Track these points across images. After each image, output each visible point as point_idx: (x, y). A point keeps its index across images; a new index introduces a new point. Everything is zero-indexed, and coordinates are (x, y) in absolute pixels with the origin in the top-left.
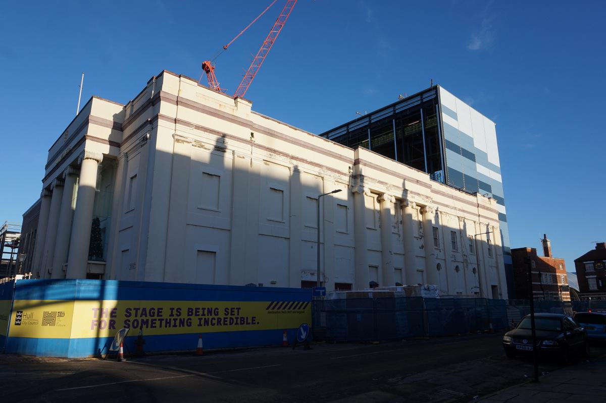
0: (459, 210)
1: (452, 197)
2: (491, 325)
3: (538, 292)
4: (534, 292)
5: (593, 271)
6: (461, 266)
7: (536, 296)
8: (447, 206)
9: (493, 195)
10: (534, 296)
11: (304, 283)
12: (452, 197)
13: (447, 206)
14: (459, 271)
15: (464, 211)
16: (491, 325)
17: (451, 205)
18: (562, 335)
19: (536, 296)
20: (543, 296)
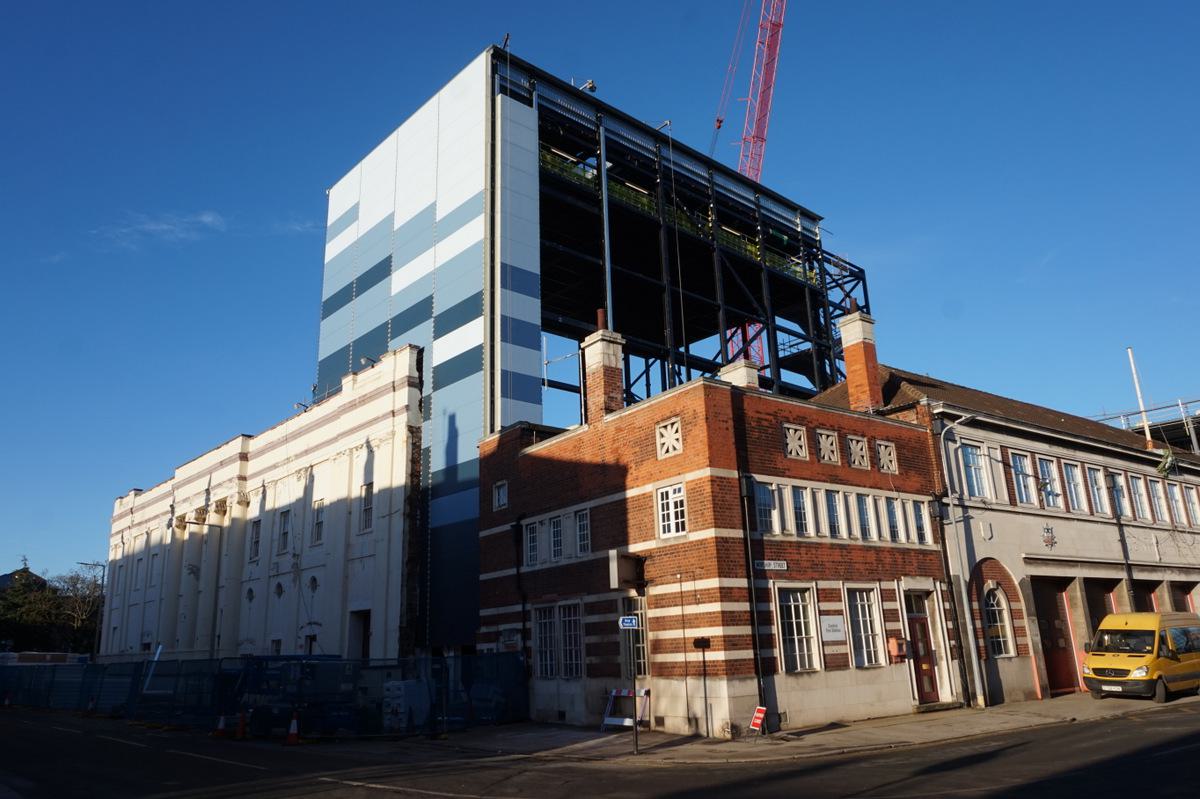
0: (297, 456)
1: (286, 440)
2: (294, 723)
3: (502, 610)
4: (483, 613)
5: (978, 559)
6: (286, 581)
7: (493, 629)
8: (275, 467)
9: (429, 397)
10: (484, 630)
11: (820, 449)
12: (286, 440)
13: (275, 467)
14: (254, 600)
15: (306, 452)
16: (294, 723)
17: (278, 460)
18: (418, 522)
19: (493, 629)
20: (519, 626)
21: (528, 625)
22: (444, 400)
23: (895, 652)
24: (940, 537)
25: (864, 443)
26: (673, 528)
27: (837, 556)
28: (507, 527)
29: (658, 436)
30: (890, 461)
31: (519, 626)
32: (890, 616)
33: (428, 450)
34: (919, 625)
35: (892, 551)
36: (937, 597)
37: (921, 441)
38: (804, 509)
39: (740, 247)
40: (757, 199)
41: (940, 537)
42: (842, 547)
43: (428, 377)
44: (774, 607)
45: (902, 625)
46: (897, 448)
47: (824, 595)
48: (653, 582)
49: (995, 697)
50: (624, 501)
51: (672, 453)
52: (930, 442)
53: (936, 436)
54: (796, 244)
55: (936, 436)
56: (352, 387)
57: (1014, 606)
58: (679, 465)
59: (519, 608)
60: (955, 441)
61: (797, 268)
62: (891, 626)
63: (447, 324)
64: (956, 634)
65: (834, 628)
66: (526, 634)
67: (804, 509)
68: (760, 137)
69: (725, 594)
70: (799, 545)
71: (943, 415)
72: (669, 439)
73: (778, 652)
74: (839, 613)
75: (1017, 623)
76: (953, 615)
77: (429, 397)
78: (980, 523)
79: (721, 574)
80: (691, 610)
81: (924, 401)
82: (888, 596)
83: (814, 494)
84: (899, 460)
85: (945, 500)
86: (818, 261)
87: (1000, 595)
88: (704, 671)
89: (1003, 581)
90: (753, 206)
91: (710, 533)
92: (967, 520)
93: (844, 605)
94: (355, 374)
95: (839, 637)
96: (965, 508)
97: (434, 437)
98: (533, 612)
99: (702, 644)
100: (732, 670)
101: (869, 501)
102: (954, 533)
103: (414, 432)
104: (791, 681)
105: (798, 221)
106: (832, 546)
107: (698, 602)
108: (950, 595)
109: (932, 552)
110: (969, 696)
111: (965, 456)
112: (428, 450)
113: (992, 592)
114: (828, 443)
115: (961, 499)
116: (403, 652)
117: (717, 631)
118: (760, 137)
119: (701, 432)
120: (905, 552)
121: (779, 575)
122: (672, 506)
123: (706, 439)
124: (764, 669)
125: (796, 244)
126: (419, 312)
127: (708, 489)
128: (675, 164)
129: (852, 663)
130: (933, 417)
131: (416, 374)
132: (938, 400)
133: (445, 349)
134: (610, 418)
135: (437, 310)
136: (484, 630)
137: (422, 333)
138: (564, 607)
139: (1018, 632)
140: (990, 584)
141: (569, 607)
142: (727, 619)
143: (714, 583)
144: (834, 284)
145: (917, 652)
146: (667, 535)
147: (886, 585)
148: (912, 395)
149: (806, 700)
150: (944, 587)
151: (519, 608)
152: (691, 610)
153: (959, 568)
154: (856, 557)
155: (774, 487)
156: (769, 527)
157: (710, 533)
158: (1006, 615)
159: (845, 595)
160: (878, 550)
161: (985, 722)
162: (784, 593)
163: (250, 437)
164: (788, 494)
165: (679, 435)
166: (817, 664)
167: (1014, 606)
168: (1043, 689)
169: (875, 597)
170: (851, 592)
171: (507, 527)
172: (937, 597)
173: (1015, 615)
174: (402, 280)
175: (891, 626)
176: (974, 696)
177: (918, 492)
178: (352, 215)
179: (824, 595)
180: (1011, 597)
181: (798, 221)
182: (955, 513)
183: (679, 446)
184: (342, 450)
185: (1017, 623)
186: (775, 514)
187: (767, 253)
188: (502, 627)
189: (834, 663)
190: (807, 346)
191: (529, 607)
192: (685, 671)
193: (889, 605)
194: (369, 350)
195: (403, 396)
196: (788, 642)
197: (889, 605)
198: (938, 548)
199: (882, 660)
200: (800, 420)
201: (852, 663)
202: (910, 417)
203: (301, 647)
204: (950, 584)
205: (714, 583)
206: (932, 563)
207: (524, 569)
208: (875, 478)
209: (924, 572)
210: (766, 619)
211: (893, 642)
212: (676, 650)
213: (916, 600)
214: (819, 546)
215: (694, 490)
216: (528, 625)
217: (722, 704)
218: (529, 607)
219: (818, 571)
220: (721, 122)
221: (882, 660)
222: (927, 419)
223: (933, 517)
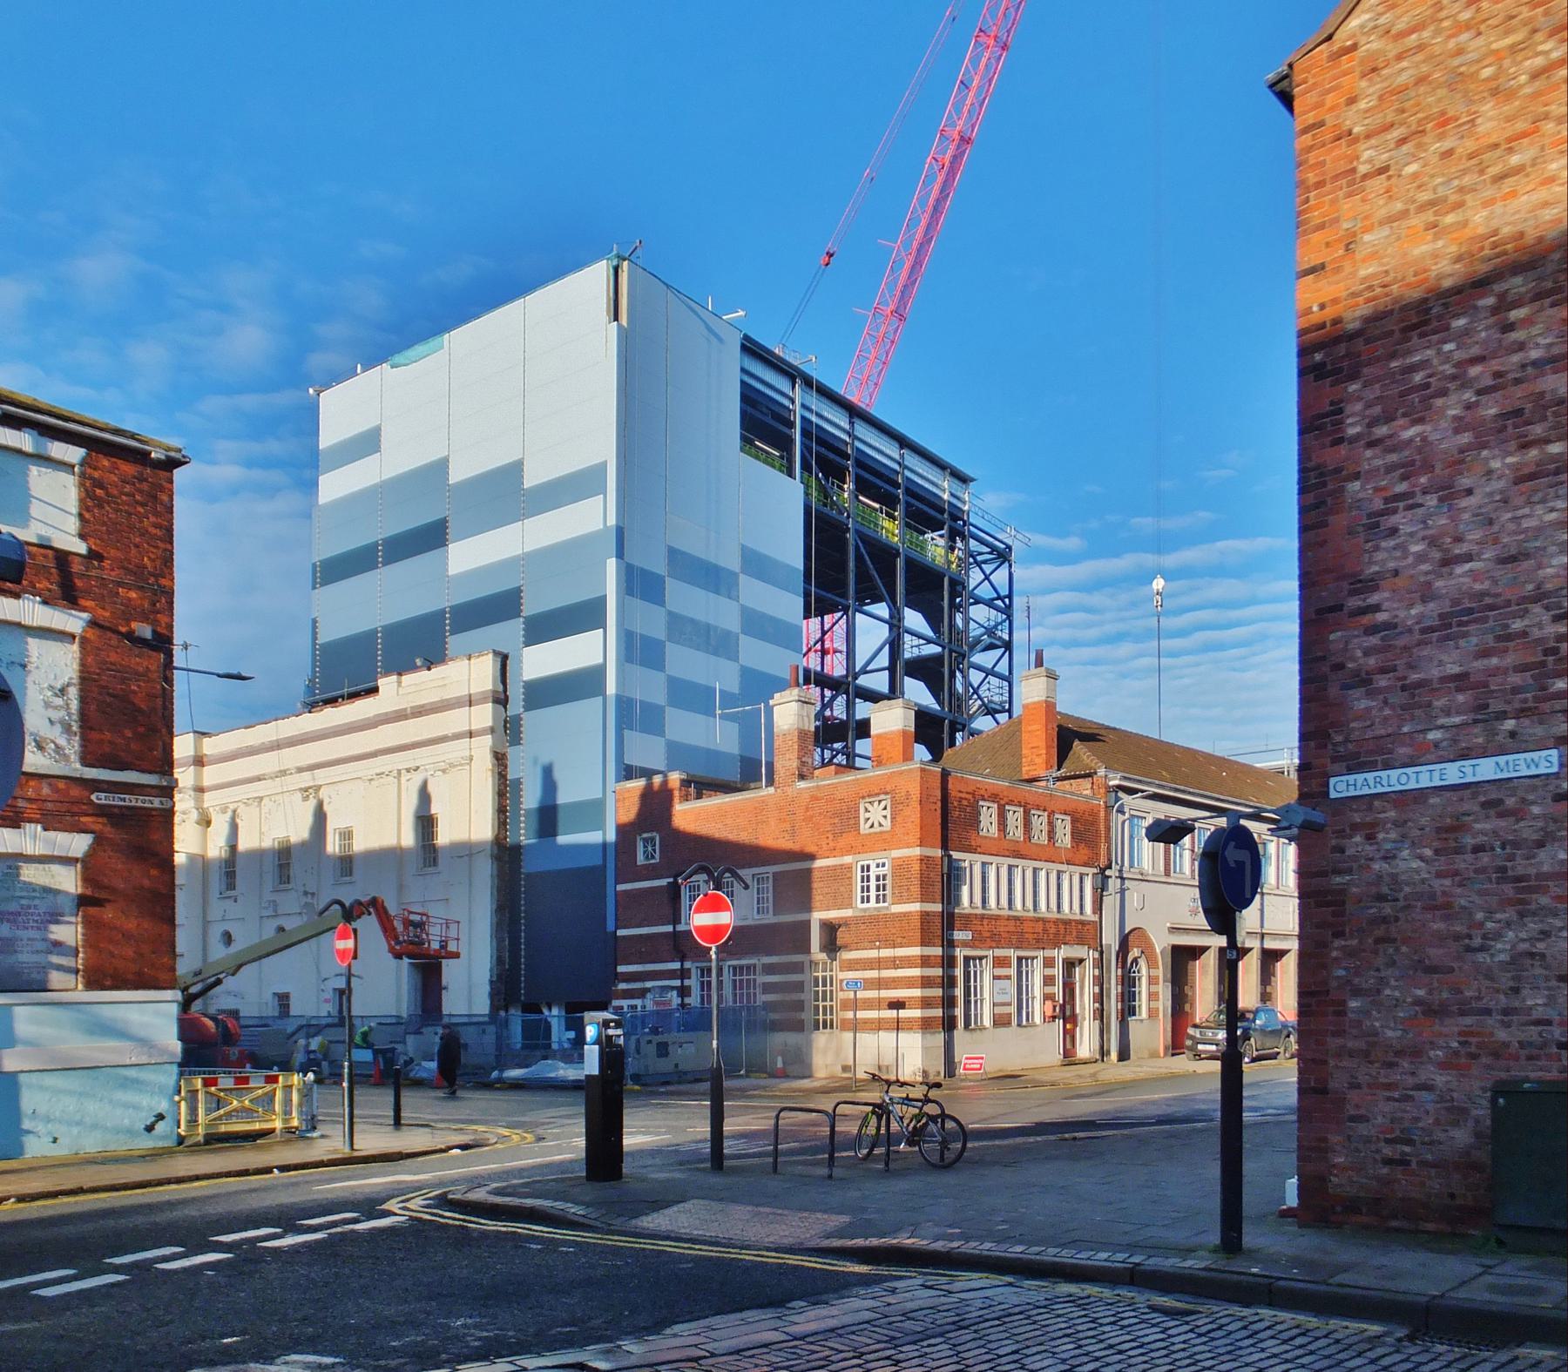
4: (620, 969)
10: (622, 986)
20: (677, 983)
21: (687, 982)
22: (534, 723)
23: (1049, 1013)
24: (1098, 907)
25: (1044, 818)
26: (873, 899)
27: (1011, 927)
28: (664, 882)
29: (862, 810)
30: (1064, 838)
31: (677, 983)
32: (1049, 980)
33: (518, 782)
34: (1069, 988)
35: (1056, 922)
36: (1089, 964)
37: (1094, 814)
38: (990, 886)
39: (876, 525)
40: (902, 456)
41: (1098, 907)
42: (1017, 919)
43: (516, 695)
44: (959, 972)
45: (1058, 990)
46: (1073, 822)
47: (1001, 962)
48: (846, 947)
49: (1124, 1055)
50: (809, 871)
51: (877, 829)
52: (1102, 814)
53: (1108, 808)
54: (939, 516)
55: (1108, 808)
56: (393, 691)
57: (1153, 972)
58: (882, 841)
59: (676, 965)
60: (1123, 813)
61: (935, 547)
62: (1049, 990)
63: (545, 628)
64: (1100, 998)
65: (1003, 992)
66: (684, 992)
67: (990, 886)
68: (899, 314)
69: (925, 962)
70: (983, 917)
71: (1120, 788)
72: (875, 815)
73: (959, 1012)
74: (1008, 977)
75: (1153, 989)
76: (1100, 981)
77: (518, 718)
78: (1133, 899)
79: (923, 944)
80: (886, 973)
81: (1102, 772)
82: (1049, 963)
83: (998, 867)
84: (1072, 833)
85: (1108, 873)
86: (963, 538)
87: (1142, 963)
88: (898, 1026)
89: (1148, 950)
90: (896, 467)
91: (915, 907)
92: (1122, 891)
93: (1013, 971)
94: (400, 674)
95: (1006, 999)
96: (1122, 879)
97: (524, 769)
98: (693, 971)
99: (897, 1005)
100: (926, 1025)
101: (1043, 874)
102: (1111, 902)
103: (500, 758)
104: (967, 1034)
105: (946, 484)
106: (1009, 918)
107: (896, 967)
108: (1100, 963)
109: (1089, 923)
110: (1104, 1053)
111: (1131, 827)
112: (518, 782)
113: (1135, 960)
114: (1015, 817)
115: (1121, 871)
116: (494, 1008)
117: (917, 993)
118: (899, 314)
119: (913, 813)
120: (1067, 922)
121: (965, 944)
122: (873, 879)
123: (918, 821)
124: (949, 1024)
125: (939, 516)
126: (493, 608)
127: (917, 867)
128: (819, 415)
129: (1014, 1022)
130: (1109, 789)
131: (501, 688)
132: (1116, 770)
133: (543, 660)
134: (802, 785)
135: (530, 607)
136: (622, 986)
137: (509, 632)
138: (735, 968)
139: (1152, 996)
140: (1134, 953)
141: (741, 968)
142: (926, 982)
143: (916, 951)
144: (979, 558)
145: (1066, 1015)
146: (865, 905)
147: (1048, 953)
148: (1087, 761)
149: (981, 1051)
150: (1097, 955)
151: (676, 965)
152: (886, 973)
153: (1110, 938)
154: (1027, 927)
155: (967, 864)
156: (958, 902)
157: (915, 907)
158: (1144, 981)
159: (1014, 962)
160: (1044, 920)
161: (1113, 1070)
162: (967, 959)
163: (204, 734)
164: (977, 869)
165: (888, 813)
166: (987, 1022)
167: (1153, 972)
168: (1166, 1048)
169: (1038, 963)
170: (1020, 959)
171: (664, 882)
172: (1089, 964)
173: (1152, 981)
174: (471, 556)
175: (1049, 990)
176: (1109, 1053)
177: (1085, 865)
178: (368, 443)
179: (1001, 962)
180: (1152, 964)
181: (946, 484)
182: (1113, 884)
183: (887, 824)
184: (386, 769)
185: (1153, 989)
186: (965, 890)
187: (908, 531)
188: (649, 984)
189: (1000, 1021)
190: (934, 649)
191: (687, 965)
192: (879, 1026)
193: (1049, 972)
194: (420, 644)
195: (484, 715)
196: (967, 1003)
197: (1049, 972)
198: (1096, 918)
199: (1038, 1019)
200: (994, 797)
201: (1014, 1022)
202: (1084, 787)
203: (327, 1001)
204: (1102, 953)
205: (916, 951)
206: (1085, 932)
207: (680, 928)
208: (1049, 854)
209: (1081, 941)
210: (949, 982)
211: (1049, 1004)
212: (870, 1008)
213: (1070, 965)
214: (997, 918)
215: (900, 867)
216: (687, 982)
217: (911, 1055)
218: (687, 965)
219: (996, 940)
220: (830, 255)
221: (1038, 1019)
222: (1102, 791)
223: (1095, 889)
